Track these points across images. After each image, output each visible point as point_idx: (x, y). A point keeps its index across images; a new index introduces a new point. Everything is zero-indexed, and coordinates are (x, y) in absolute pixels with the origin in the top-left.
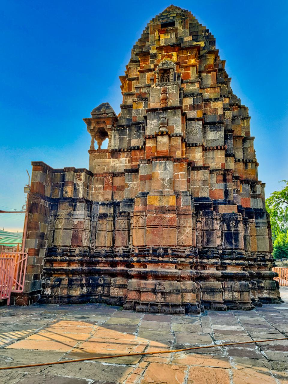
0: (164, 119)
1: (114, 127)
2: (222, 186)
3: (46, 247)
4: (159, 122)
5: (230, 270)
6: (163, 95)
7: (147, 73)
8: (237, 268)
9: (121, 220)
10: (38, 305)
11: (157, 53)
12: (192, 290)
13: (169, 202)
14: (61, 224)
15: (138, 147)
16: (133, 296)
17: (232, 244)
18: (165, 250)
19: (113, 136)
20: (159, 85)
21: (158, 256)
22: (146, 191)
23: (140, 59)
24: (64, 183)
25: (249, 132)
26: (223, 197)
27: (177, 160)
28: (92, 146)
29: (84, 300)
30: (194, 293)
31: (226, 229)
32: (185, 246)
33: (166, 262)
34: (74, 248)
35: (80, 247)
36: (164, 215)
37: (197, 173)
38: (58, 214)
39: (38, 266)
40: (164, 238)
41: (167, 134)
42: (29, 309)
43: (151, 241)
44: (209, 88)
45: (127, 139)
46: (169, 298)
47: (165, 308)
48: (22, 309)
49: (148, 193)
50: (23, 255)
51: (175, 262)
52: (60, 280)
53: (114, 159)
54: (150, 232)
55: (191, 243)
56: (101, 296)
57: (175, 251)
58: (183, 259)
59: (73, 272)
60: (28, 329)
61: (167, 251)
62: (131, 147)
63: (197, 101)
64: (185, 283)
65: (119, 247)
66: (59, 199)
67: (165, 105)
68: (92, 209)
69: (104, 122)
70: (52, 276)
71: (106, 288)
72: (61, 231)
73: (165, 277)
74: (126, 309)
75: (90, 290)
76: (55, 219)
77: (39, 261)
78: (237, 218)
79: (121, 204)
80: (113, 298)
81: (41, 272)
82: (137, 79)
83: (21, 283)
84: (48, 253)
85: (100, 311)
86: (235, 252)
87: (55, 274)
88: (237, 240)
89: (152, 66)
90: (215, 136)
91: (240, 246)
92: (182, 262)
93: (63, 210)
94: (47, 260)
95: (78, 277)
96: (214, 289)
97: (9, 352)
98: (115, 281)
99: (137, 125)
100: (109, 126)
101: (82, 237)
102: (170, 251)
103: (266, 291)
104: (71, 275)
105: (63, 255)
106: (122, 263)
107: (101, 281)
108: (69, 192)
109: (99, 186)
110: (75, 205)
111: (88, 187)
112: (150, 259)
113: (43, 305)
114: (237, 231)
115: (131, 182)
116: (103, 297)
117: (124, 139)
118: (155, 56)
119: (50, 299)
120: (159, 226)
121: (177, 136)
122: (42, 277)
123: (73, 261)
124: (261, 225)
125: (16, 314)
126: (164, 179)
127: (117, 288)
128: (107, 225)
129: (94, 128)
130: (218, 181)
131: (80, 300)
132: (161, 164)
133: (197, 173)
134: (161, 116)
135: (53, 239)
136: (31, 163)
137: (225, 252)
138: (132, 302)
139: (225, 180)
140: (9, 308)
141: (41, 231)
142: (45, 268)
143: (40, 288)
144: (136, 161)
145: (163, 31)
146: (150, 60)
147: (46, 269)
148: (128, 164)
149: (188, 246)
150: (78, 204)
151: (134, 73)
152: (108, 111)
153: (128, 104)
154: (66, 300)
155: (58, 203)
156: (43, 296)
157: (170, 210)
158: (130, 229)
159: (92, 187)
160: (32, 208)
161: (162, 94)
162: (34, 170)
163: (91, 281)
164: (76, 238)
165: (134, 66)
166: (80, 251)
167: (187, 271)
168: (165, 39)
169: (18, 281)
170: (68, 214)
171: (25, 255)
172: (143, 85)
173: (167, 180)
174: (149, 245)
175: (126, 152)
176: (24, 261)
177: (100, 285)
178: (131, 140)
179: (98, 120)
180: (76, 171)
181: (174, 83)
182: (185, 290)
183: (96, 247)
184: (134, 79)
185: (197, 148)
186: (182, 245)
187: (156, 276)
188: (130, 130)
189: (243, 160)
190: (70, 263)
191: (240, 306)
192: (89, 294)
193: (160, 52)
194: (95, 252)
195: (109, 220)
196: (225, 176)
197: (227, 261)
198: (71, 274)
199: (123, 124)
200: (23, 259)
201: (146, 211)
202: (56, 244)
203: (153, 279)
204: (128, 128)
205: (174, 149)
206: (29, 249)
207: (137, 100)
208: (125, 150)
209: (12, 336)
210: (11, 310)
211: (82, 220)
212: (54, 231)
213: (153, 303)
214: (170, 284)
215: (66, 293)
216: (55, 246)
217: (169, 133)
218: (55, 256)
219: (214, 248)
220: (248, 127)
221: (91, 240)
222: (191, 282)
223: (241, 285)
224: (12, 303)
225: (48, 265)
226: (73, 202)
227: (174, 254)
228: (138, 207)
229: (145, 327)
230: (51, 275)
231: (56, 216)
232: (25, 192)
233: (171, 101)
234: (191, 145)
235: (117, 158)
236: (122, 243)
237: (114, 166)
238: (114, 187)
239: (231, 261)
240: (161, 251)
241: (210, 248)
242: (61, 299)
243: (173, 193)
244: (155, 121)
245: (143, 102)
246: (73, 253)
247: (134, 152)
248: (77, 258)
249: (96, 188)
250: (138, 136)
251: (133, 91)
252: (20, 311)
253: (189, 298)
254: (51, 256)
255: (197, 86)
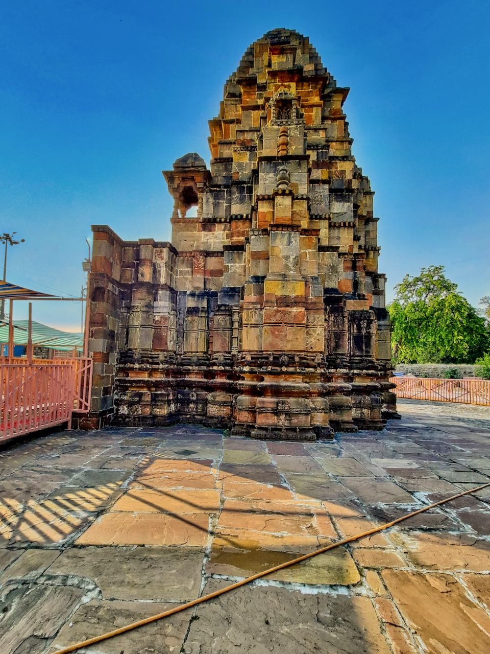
0: (285, 172)
1: (206, 186)
2: (350, 274)
3: (118, 351)
4: (279, 176)
5: (358, 382)
6: (282, 137)
7: (252, 112)
8: (366, 380)
9: (220, 317)
10: (111, 428)
11: (268, 82)
12: (323, 409)
13: (295, 291)
14: (137, 319)
15: (242, 216)
16: (244, 417)
17: (361, 350)
18: (290, 358)
19: (204, 200)
20: (276, 122)
21: (281, 366)
22: (260, 274)
23: (242, 91)
24: (138, 262)
25: (372, 212)
26: (351, 290)
27: (305, 232)
28: (176, 213)
29: (173, 420)
30: (325, 413)
31: (355, 331)
32: (315, 352)
33: (292, 373)
34: (156, 353)
35: (164, 351)
36: (288, 309)
37: (323, 255)
38: (132, 304)
39: (108, 376)
40: (288, 341)
41: (291, 193)
42: (102, 436)
43: (271, 345)
44: (334, 141)
45: (225, 205)
46: (295, 421)
47: (290, 434)
48: (91, 436)
49: (264, 277)
50: (86, 362)
51: (304, 373)
52: (140, 395)
53: (206, 233)
54: (269, 332)
55: (322, 348)
56: (194, 415)
57: (304, 358)
58: (312, 370)
59: (157, 385)
60: (110, 482)
61: (293, 358)
62: (232, 216)
63: (322, 156)
64: (314, 400)
65: (218, 352)
66: (132, 285)
67: (285, 152)
68: (178, 301)
69: (193, 179)
70: (128, 390)
71: (200, 406)
72: (138, 329)
73: (289, 392)
74: (236, 434)
75: (179, 408)
76: (128, 313)
77: (109, 370)
78: (370, 317)
79: (219, 294)
80: (212, 418)
81: (112, 384)
82: (238, 121)
83: (87, 400)
84: (120, 359)
85: (201, 437)
86: (366, 360)
87: (132, 387)
88: (368, 345)
89: (261, 102)
90: (341, 208)
91: (371, 351)
92: (312, 373)
93: (139, 300)
94: (119, 368)
95: (163, 392)
96: (343, 406)
97: (87, 559)
98: (214, 397)
99: (239, 184)
100: (200, 185)
101: (166, 338)
102: (297, 359)
103: (385, 405)
104: (154, 389)
105: (143, 362)
106: (223, 373)
107: (193, 396)
108: (146, 274)
109: (186, 269)
110: (156, 294)
111: (172, 269)
112: (269, 370)
113: (119, 429)
114: (369, 333)
115: (232, 264)
116: (196, 417)
117: (221, 204)
118: (263, 88)
119: (127, 419)
120: (281, 323)
121: (302, 198)
122: (114, 391)
123: (156, 370)
124: (383, 328)
125: (84, 447)
126: (287, 258)
127: (217, 406)
128: (198, 323)
129: (178, 186)
130: (346, 269)
131: (168, 421)
132: (283, 235)
133: (323, 255)
134: (281, 168)
135: (127, 340)
136: (90, 228)
137: (353, 359)
138: (243, 425)
139: (354, 268)
140: (72, 436)
141: (110, 328)
142: (116, 378)
143: (112, 406)
144: (238, 236)
145: (277, 49)
146: (256, 93)
147: (118, 380)
148: (225, 240)
149: (318, 352)
150: (160, 292)
151: (235, 112)
152: (197, 163)
153: (225, 156)
154: (149, 421)
155: (131, 290)
156: (117, 416)
157: (296, 303)
158: (232, 329)
159: (177, 271)
160: (96, 294)
161: (280, 137)
162: (96, 238)
163: (179, 396)
164: (158, 339)
165: (232, 102)
166: (165, 357)
167: (318, 384)
168: (279, 62)
169: (82, 397)
170: (146, 306)
171: (89, 361)
172: (247, 129)
173: (291, 259)
174: (267, 351)
175: (224, 222)
176: (89, 369)
177: (193, 402)
178: (230, 207)
179: (184, 175)
180: (155, 245)
181: (298, 122)
182: (314, 409)
183: (184, 352)
184: (232, 122)
185: (322, 221)
186: (311, 350)
187: (276, 391)
188: (230, 193)
189: (365, 246)
190: (152, 372)
191: (371, 425)
192: (178, 412)
193: (273, 81)
194: (183, 359)
195: (201, 317)
196: (354, 263)
197: (356, 371)
198: (154, 387)
199: (219, 183)
200: (87, 367)
201: (261, 303)
202: (132, 347)
203: (272, 396)
204: (225, 190)
205: (298, 217)
206: (95, 353)
207: (239, 149)
208: (223, 220)
209: (85, 504)
210: (74, 439)
211: (167, 314)
212: (127, 329)
213: (274, 427)
214: (297, 403)
215: (149, 413)
216: (130, 350)
217: (293, 192)
218: (131, 363)
219: (343, 355)
220: (371, 205)
221: (178, 343)
222: (320, 399)
223: (372, 399)
224: (74, 426)
225: (121, 374)
226: (153, 288)
227: (298, 362)
228: (250, 297)
229: (290, 469)
230: (127, 388)
231: (129, 308)
232: (85, 270)
233: (293, 148)
234: (314, 217)
235: (210, 230)
236: (223, 347)
237: (207, 242)
238: (207, 270)
239: (360, 371)
240: (285, 359)
241: (339, 354)
242: (142, 421)
243: (300, 278)
244: (271, 175)
245: (248, 153)
246: (155, 359)
247: (236, 222)
248: (161, 366)
249: (181, 272)
250: (242, 200)
251: (231, 138)
252: (88, 442)
253: (320, 419)
254: (125, 363)
255: (322, 135)
